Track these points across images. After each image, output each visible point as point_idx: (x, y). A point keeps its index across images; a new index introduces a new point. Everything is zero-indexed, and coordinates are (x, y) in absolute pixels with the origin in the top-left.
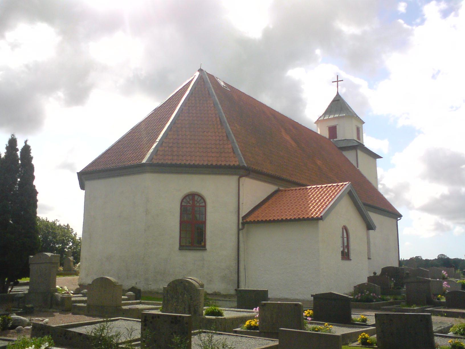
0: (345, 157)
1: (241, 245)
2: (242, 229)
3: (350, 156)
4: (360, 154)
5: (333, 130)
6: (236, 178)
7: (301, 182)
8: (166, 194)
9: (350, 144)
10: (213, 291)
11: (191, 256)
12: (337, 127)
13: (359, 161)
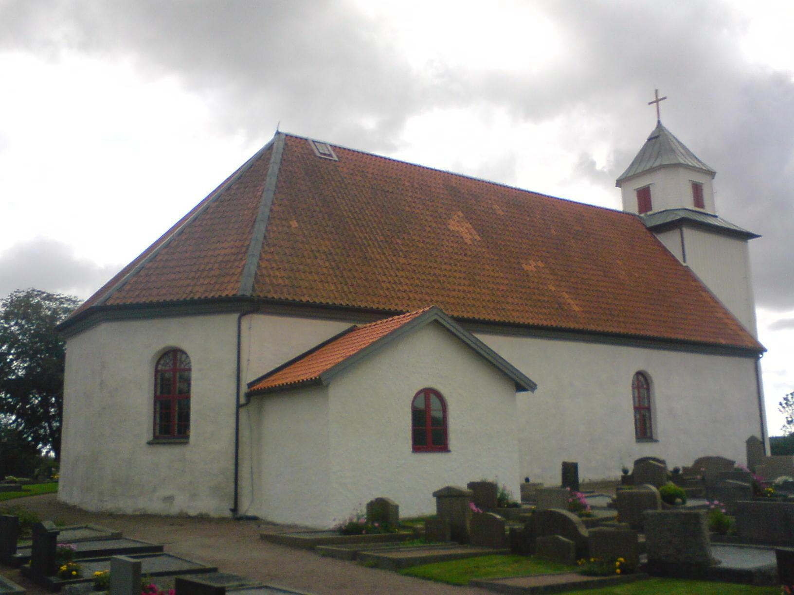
0: (660, 242)
1: (245, 433)
3: (670, 241)
4: (689, 234)
5: (644, 197)
6: (236, 316)
7: (393, 308)
9: (669, 219)
11: (167, 454)
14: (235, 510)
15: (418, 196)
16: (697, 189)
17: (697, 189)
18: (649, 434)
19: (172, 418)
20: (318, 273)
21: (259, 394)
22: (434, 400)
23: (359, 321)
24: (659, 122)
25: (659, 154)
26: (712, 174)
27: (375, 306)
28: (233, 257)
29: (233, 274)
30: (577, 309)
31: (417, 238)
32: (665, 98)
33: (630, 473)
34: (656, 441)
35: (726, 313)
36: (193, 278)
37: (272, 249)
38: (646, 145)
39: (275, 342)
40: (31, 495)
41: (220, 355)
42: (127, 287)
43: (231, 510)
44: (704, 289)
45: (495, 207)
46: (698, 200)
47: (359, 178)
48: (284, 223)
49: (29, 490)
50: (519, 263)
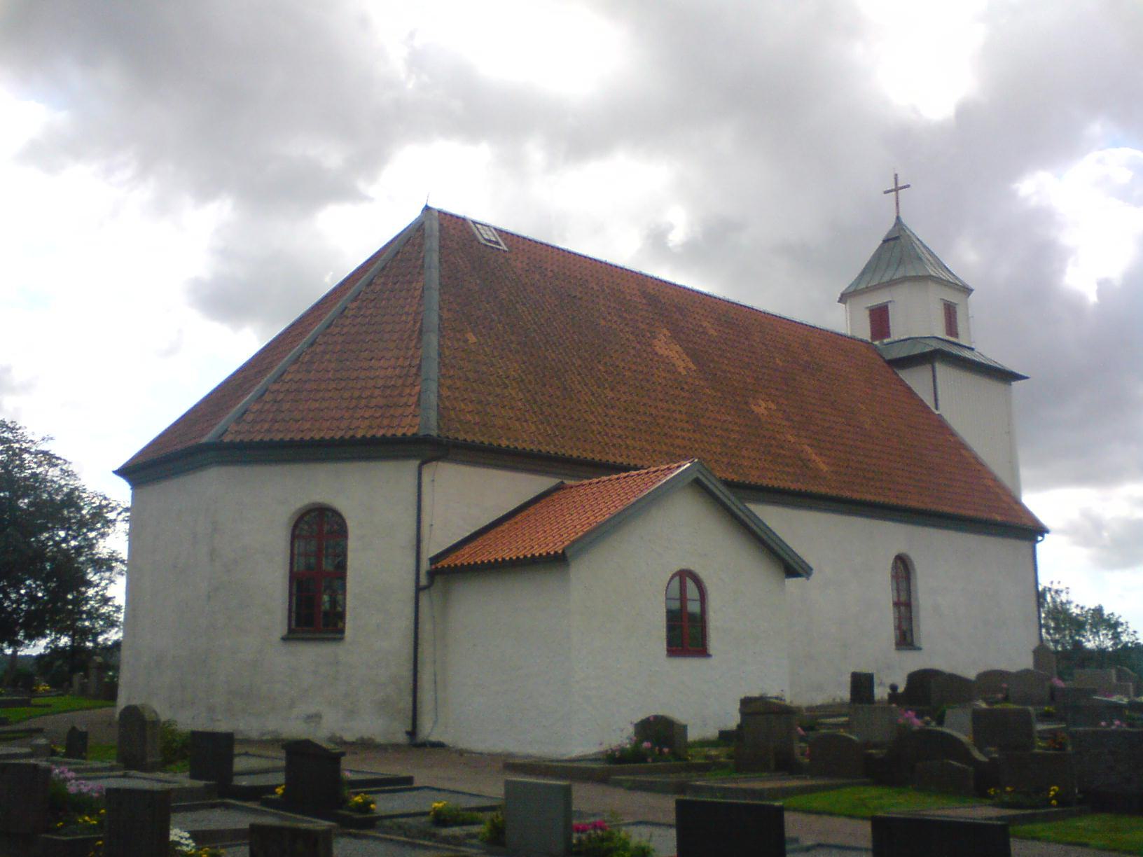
0: (902, 380)
1: (426, 627)
2: (425, 588)
3: (917, 380)
4: (942, 370)
5: (880, 318)
6: (417, 462)
8: (256, 513)
9: (917, 350)
10: (358, 736)
11: (311, 654)
12: (890, 307)
13: (940, 397)
14: (412, 733)
15: (613, 305)
16: (950, 312)
17: (950, 312)
18: (909, 640)
19: (315, 606)
20: (512, 408)
21: (445, 573)
22: (690, 584)
23: (573, 477)
24: (898, 218)
25: (900, 262)
26: (967, 291)
27: (589, 456)
28: (400, 382)
29: (406, 405)
30: (825, 468)
31: (622, 365)
32: (908, 186)
33: (901, 689)
34: (920, 649)
35: (995, 480)
36: (348, 408)
37: (452, 373)
38: (881, 247)
39: (465, 499)
40: (53, 714)
41: (391, 518)
42: (250, 417)
43: (408, 733)
44: (961, 446)
45: (705, 324)
46: (951, 327)
47: (537, 277)
48: (458, 336)
49: (48, 706)
50: (746, 403)
